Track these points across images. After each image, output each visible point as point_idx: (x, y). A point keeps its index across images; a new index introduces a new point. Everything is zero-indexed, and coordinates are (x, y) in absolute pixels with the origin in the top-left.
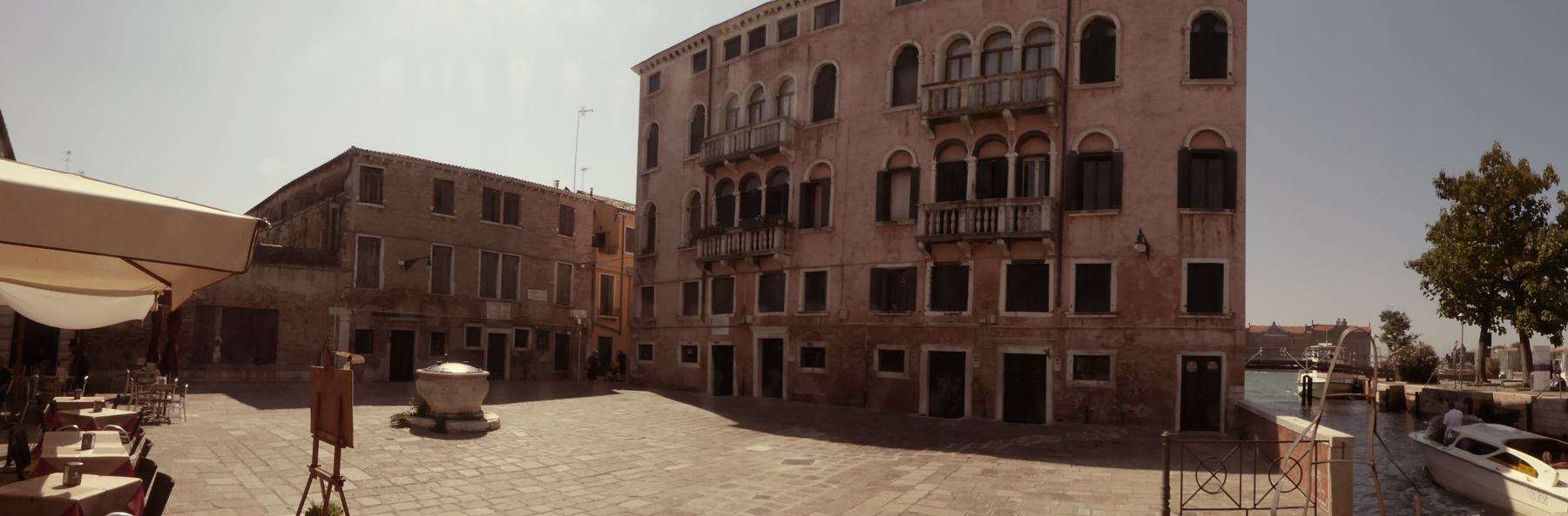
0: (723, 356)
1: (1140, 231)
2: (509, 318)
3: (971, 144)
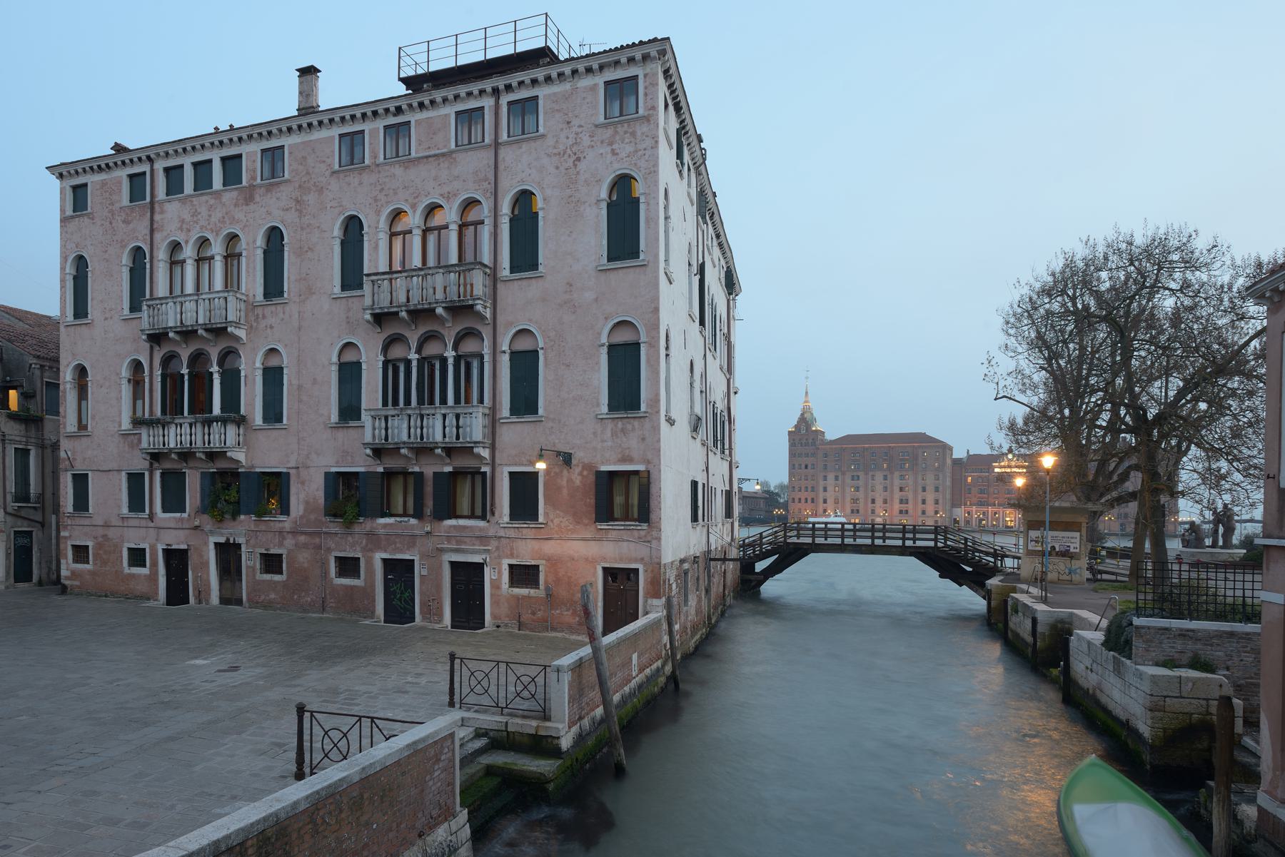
0: (177, 561)
3: (413, 339)
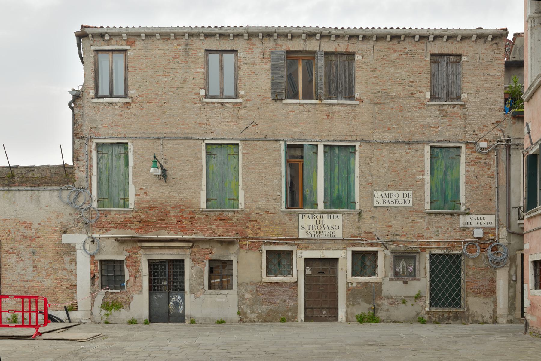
1: (155, 157)
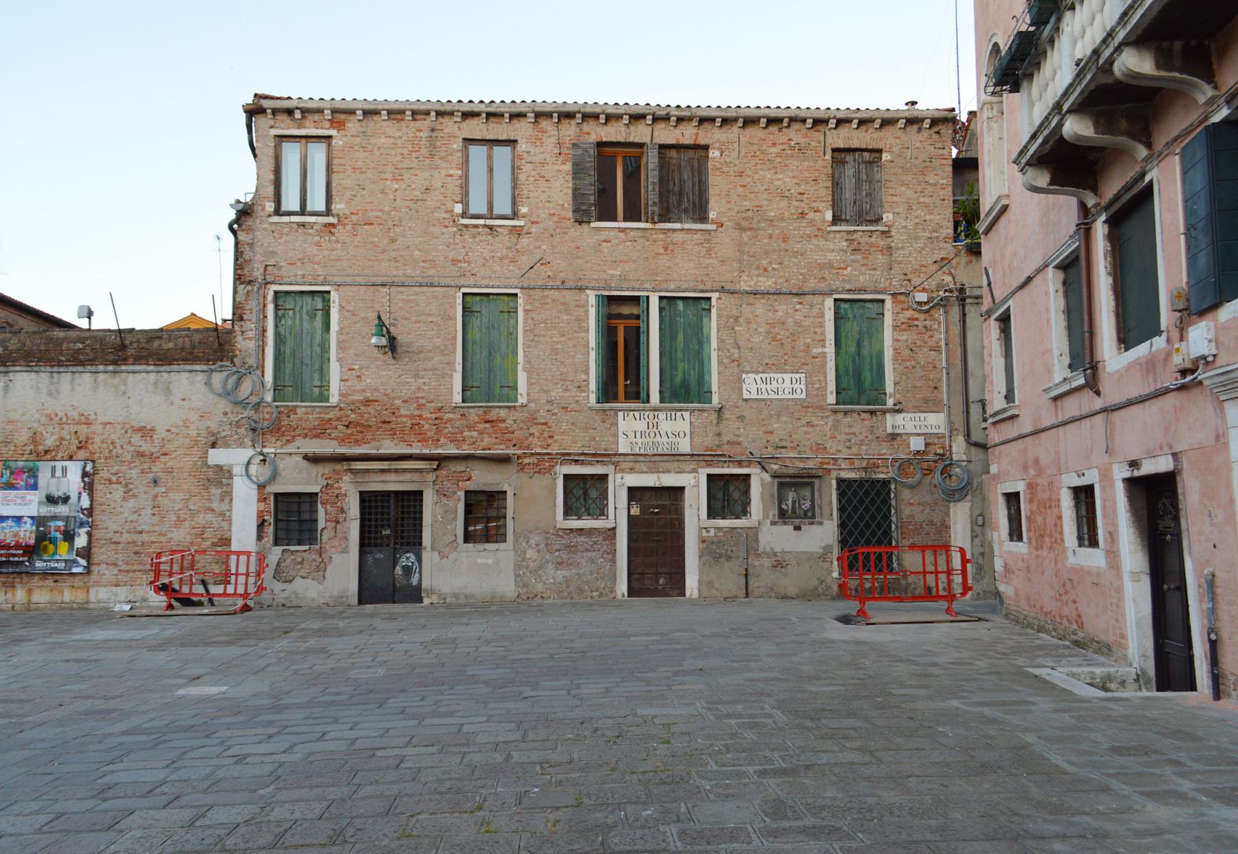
2: (685, 446)
